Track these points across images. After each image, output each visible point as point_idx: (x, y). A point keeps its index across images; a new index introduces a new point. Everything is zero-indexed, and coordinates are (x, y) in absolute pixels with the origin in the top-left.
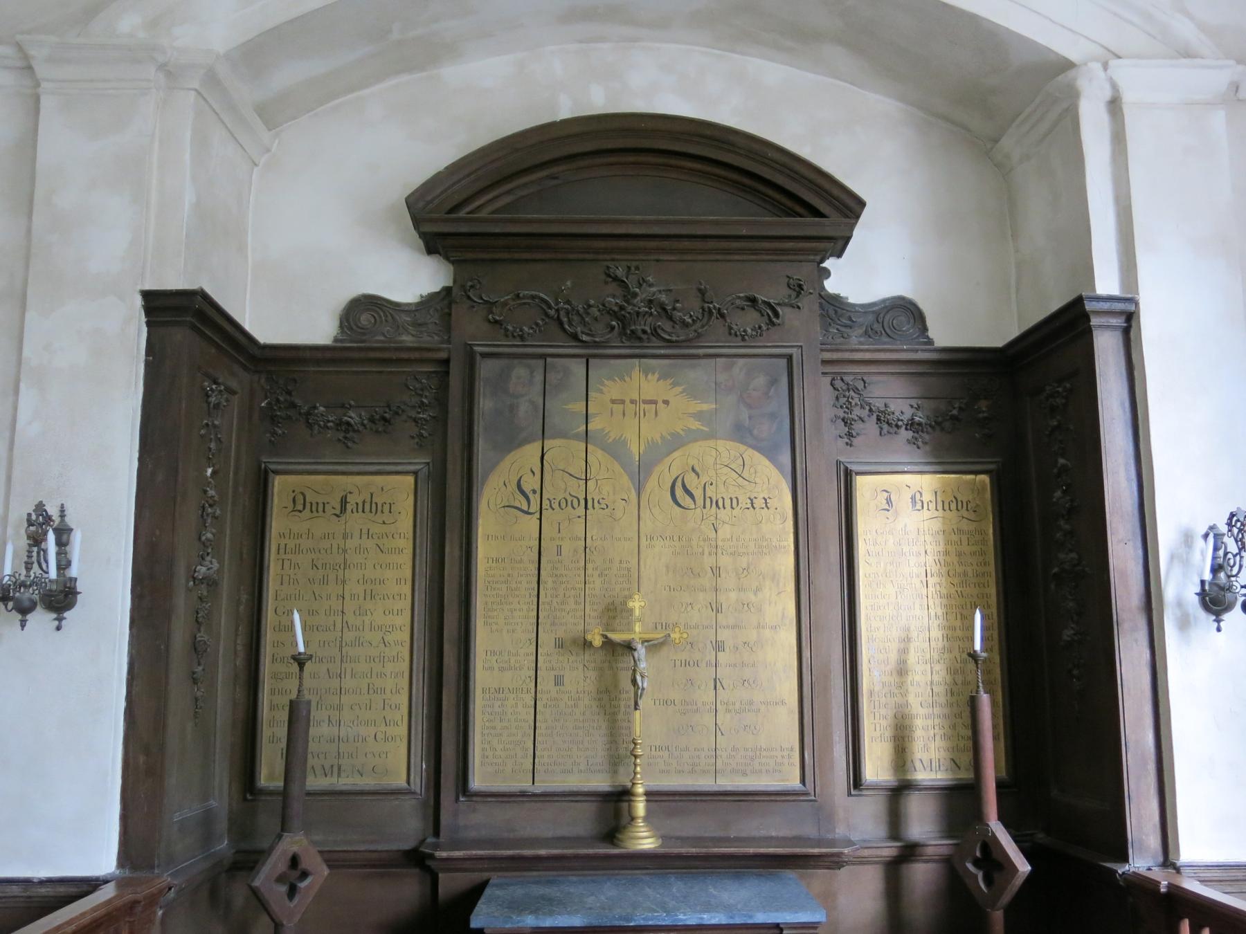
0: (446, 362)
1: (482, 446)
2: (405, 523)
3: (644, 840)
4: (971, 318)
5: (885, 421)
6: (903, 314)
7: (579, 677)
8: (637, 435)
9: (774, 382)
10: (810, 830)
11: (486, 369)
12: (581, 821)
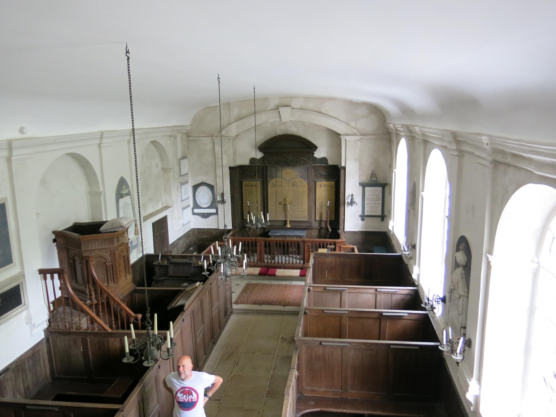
0: (263, 167)
1: (268, 179)
3: (289, 226)
5: (321, 175)
6: (324, 160)
7: (281, 207)
10: (309, 225)
11: (269, 169)
12: (282, 224)
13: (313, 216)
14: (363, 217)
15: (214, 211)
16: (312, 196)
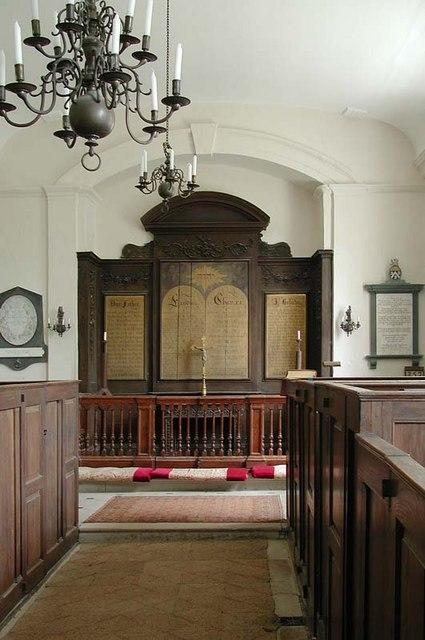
2: (142, 309)
4: (300, 251)
5: (277, 280)
6: (283, 248)
8: (205, 284)
9: (244, 268)
11: (164, 266)
13: (260, 370)
14: (373, 360)
15: (38, 352)
16: (257, 325)
